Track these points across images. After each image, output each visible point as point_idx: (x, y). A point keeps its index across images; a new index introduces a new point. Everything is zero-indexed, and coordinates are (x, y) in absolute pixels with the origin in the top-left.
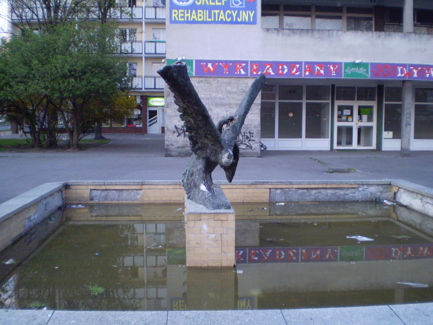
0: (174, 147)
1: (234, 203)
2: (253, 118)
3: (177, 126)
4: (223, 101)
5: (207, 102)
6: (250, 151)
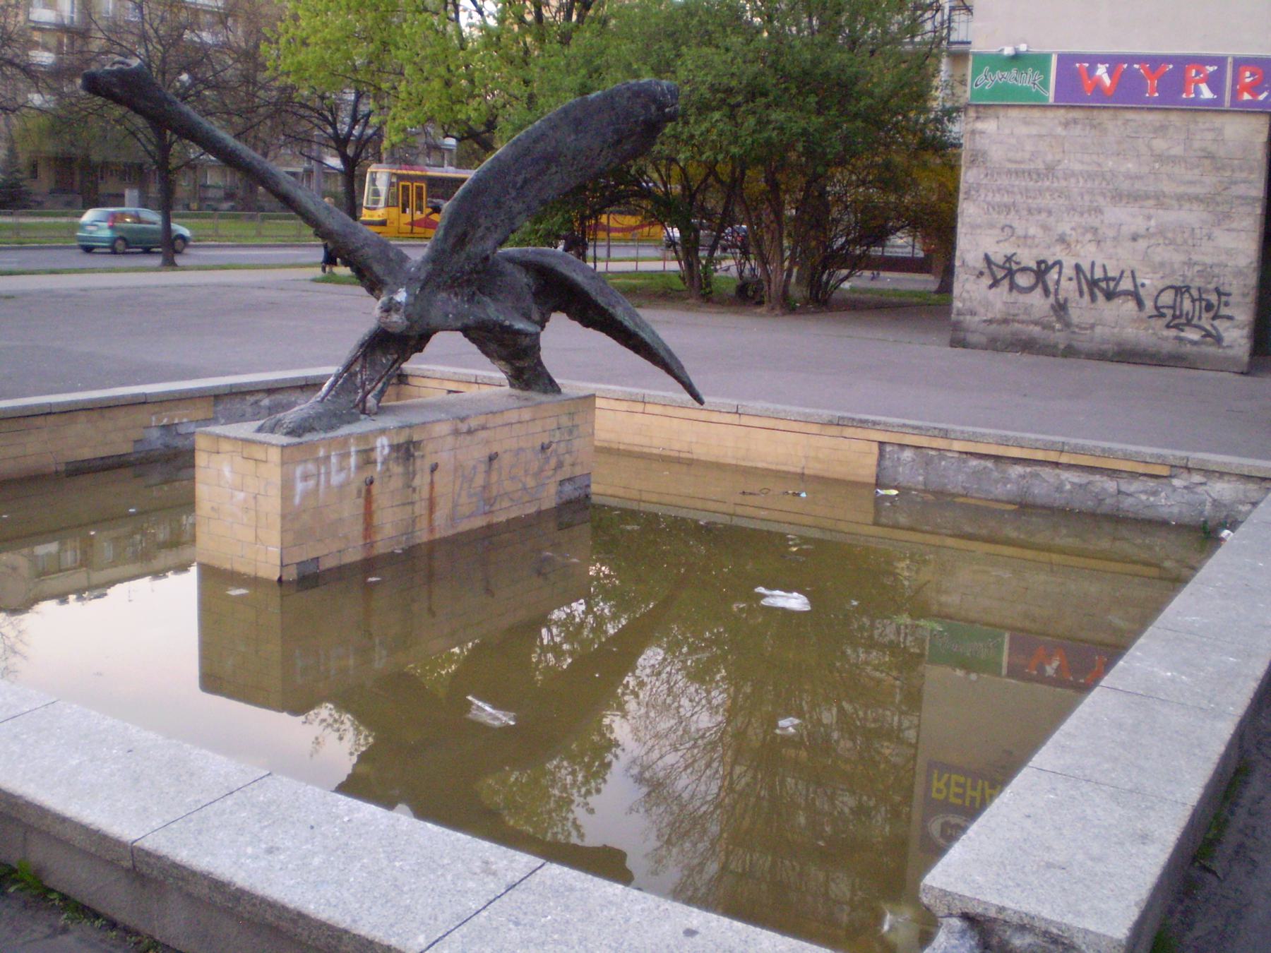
0: (977, 319)
1: (778, 471)
2: (1232, 245)
3: (993, 258)
4: (1138, 185)
5: (1089, 185)
6: (1211, 350)
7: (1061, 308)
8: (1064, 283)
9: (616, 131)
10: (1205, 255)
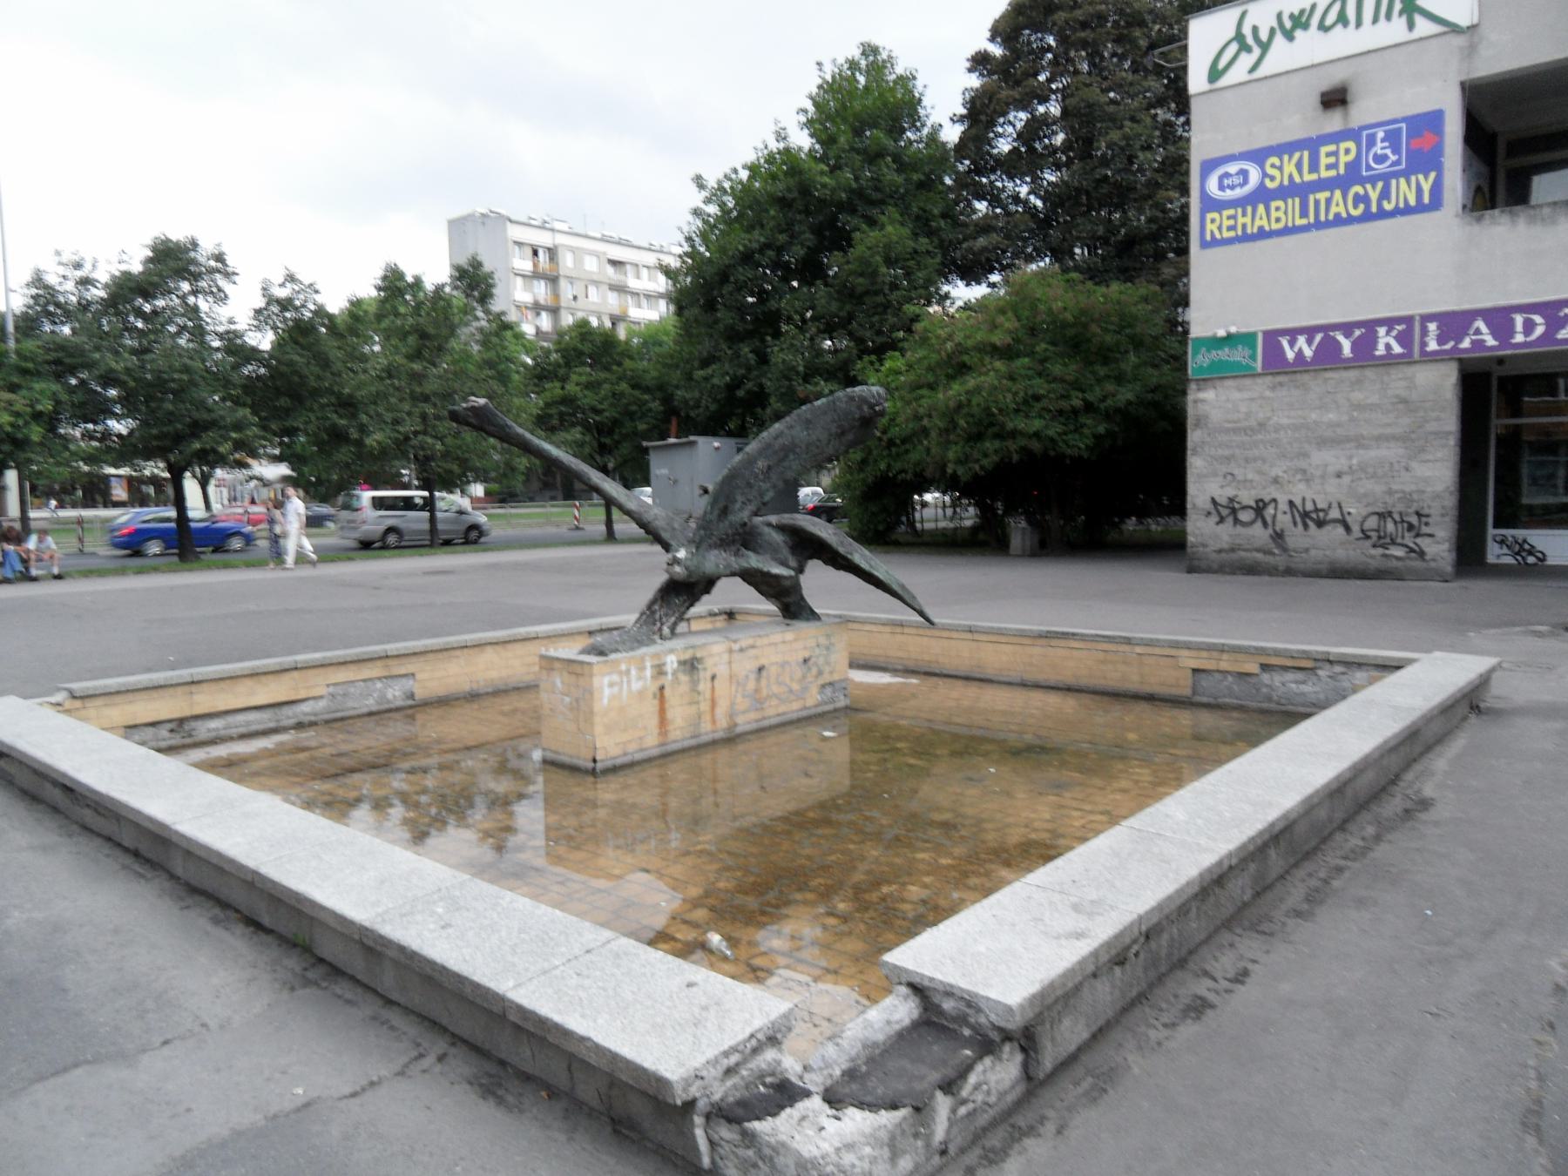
2: (1428, 474)
3: (1218, 500)
4: (1339, 431)
7: (1278, 536)
8: (1280, 517)
9: (839, 427)
10: (1404, 483)
